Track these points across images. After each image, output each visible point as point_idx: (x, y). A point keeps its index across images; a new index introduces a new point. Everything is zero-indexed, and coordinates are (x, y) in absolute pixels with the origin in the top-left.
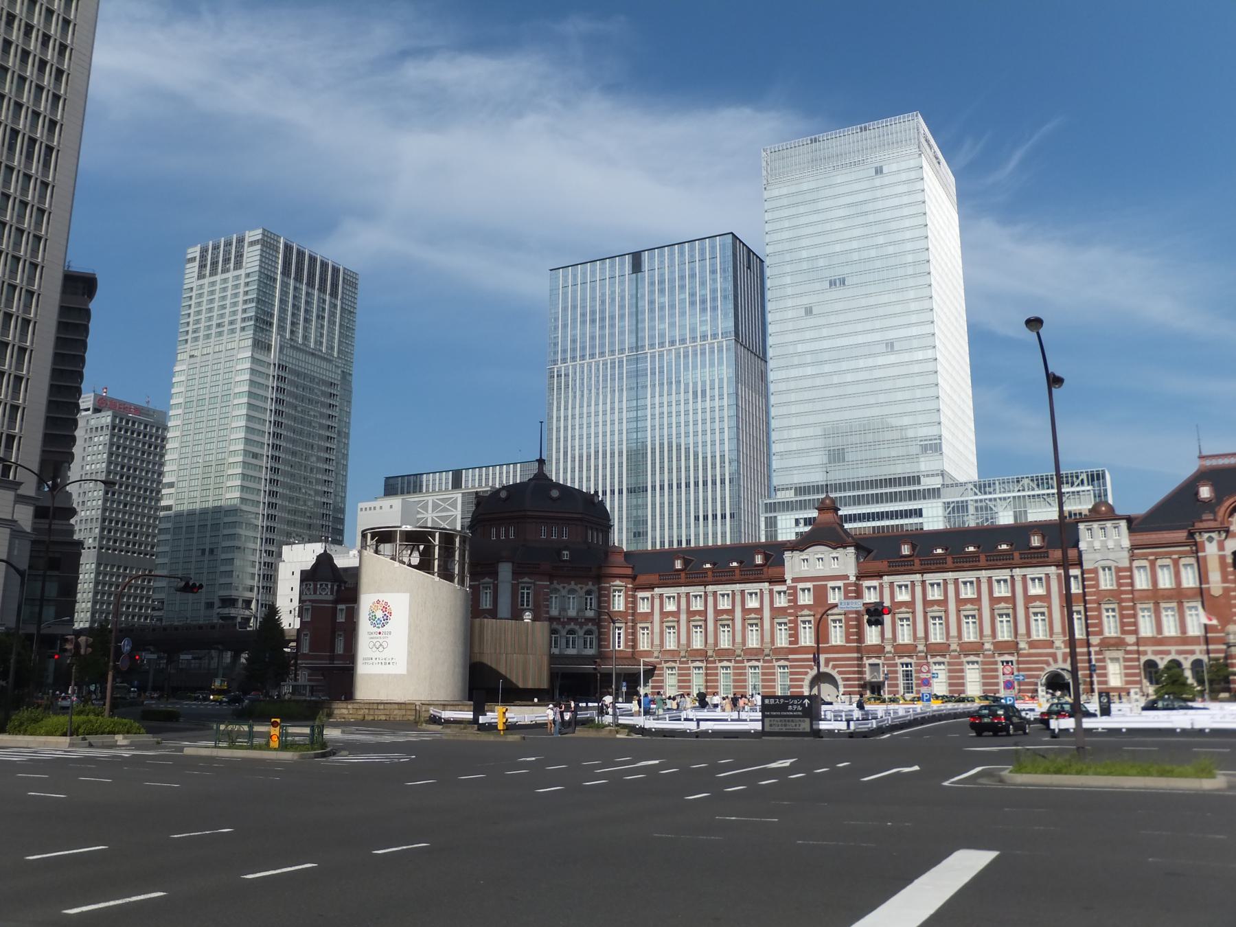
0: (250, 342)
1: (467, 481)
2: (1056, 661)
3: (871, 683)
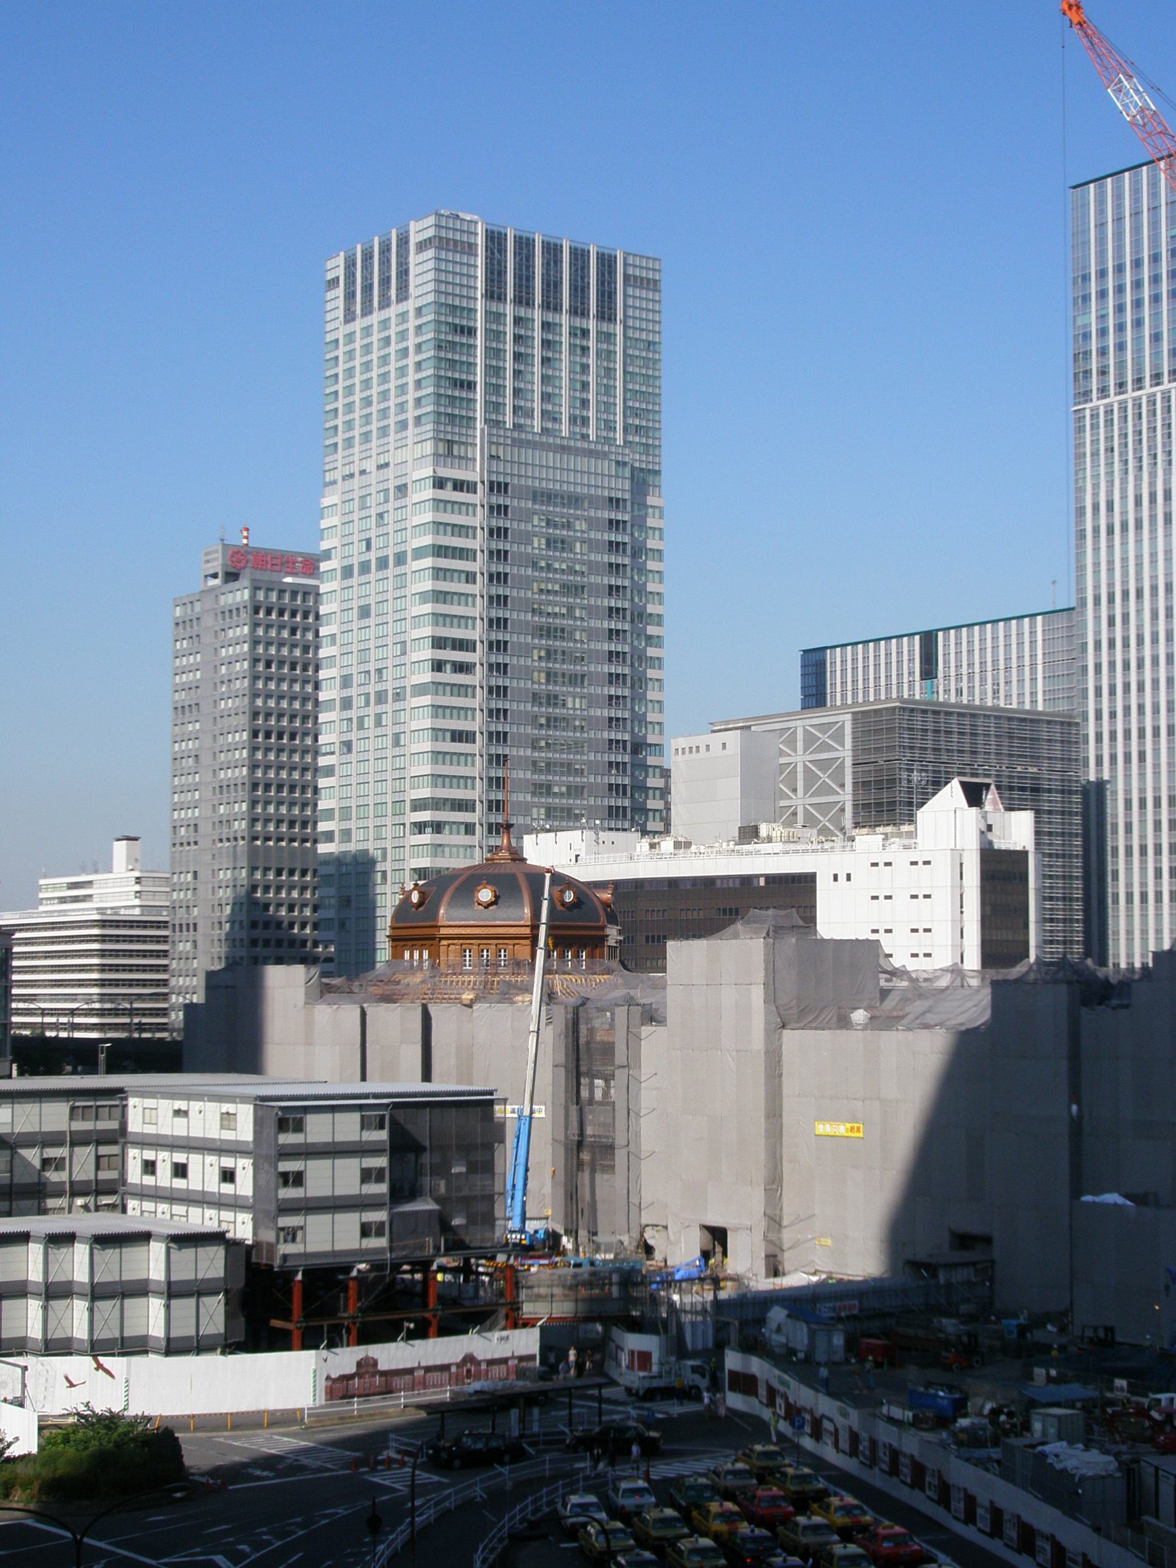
0: (429, 448)
1: (833, 693)
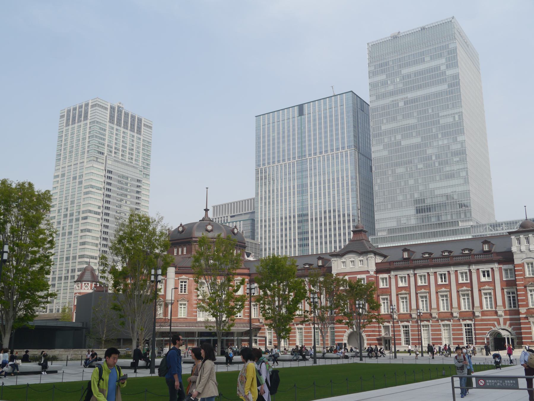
2: (499, 324)
3: (384, 338)
